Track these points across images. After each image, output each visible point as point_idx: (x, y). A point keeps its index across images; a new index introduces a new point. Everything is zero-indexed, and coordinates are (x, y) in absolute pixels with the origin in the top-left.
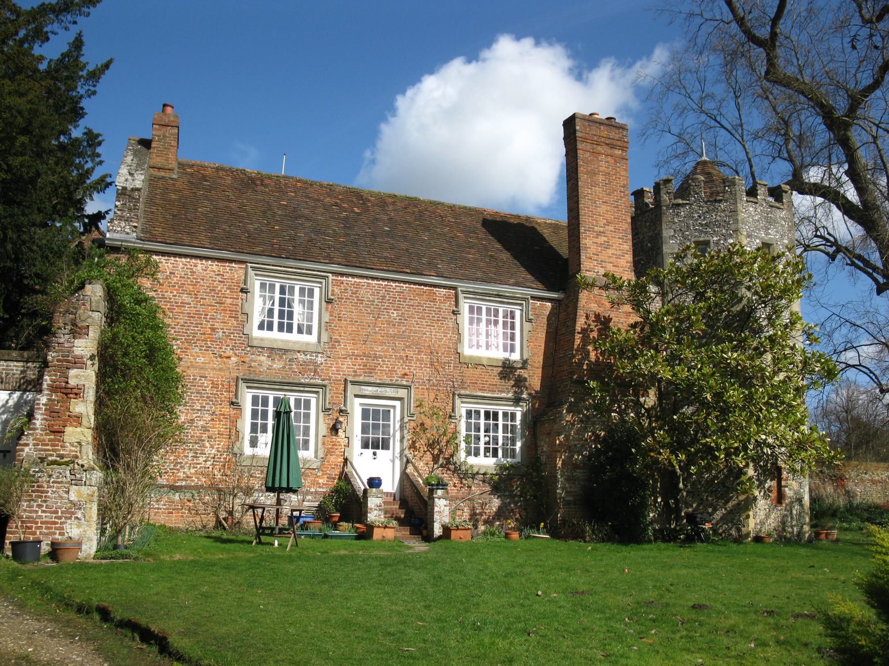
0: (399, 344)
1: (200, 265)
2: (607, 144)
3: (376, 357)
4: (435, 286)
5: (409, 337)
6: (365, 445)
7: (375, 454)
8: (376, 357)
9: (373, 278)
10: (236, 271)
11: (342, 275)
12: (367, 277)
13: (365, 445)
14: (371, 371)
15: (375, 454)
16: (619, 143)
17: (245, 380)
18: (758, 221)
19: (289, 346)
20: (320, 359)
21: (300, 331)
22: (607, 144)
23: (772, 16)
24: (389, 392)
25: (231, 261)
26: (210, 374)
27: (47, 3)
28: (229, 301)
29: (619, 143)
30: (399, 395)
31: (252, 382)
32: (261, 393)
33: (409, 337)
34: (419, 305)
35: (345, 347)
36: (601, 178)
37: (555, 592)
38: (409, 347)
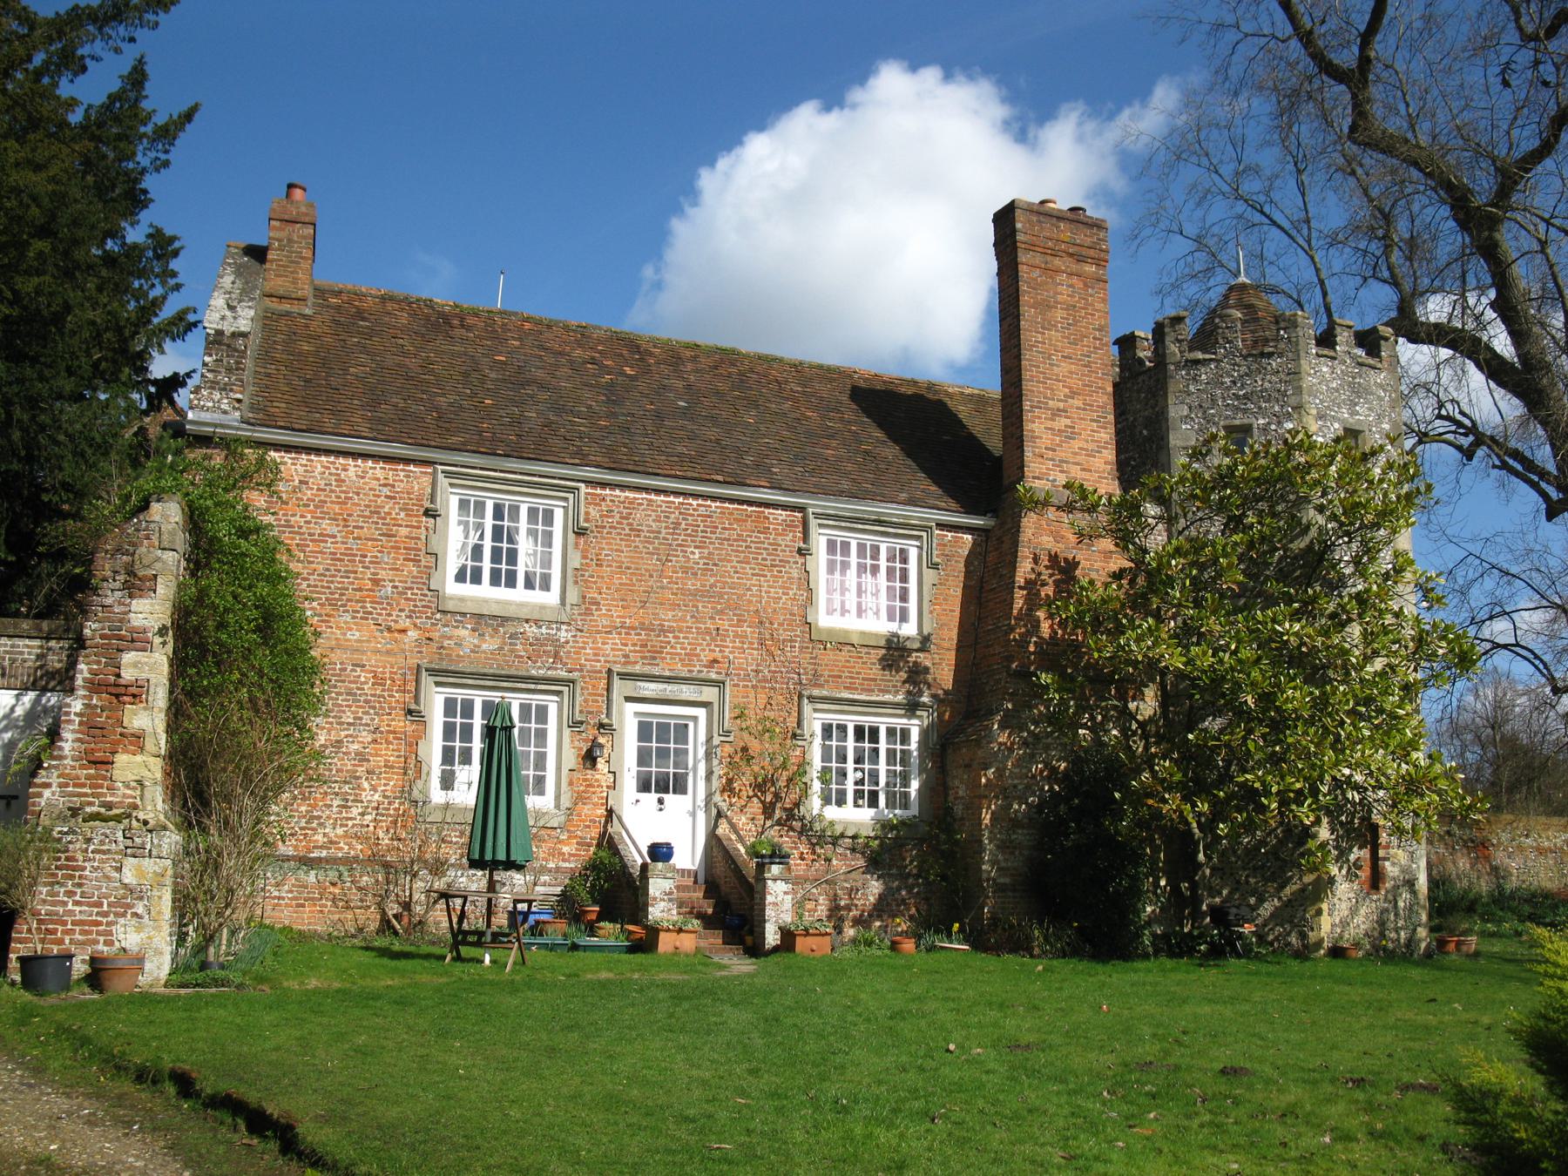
0: (704, 608)
1: (353, 468)
2: (1071, 255)
3: (663, 631)
4: (767, 505)
5: (721, 595)
6: (644, 786)
7: (661, 801)
8: (663, 631)
9: (658, 491)
10: (415, 479)
11: (603, 485)
12: (647, 490)
13: (644, 786)
14: (654, 655)
15: (661, 801)
16: (1092, 253)
17: (433, 672)
18: (1337, 390)
19: (510, 612)
20: (564, 635)
21: (529, 585)
22: (1071, 255)
23: (1362, 28)
24: (687, 692)
25: (407, 461)
26: (371, 660)
27: (82, 5)
28: (404, 531)
29: (1092, 253)
30: (703, 698)
31: (444, 675)
32: (460, 694)
33: (721, 595)
34: (740, 538)
35: (609, 613)
36: (1059, 314)
37: (979, 1045)
38: (722, 612)
